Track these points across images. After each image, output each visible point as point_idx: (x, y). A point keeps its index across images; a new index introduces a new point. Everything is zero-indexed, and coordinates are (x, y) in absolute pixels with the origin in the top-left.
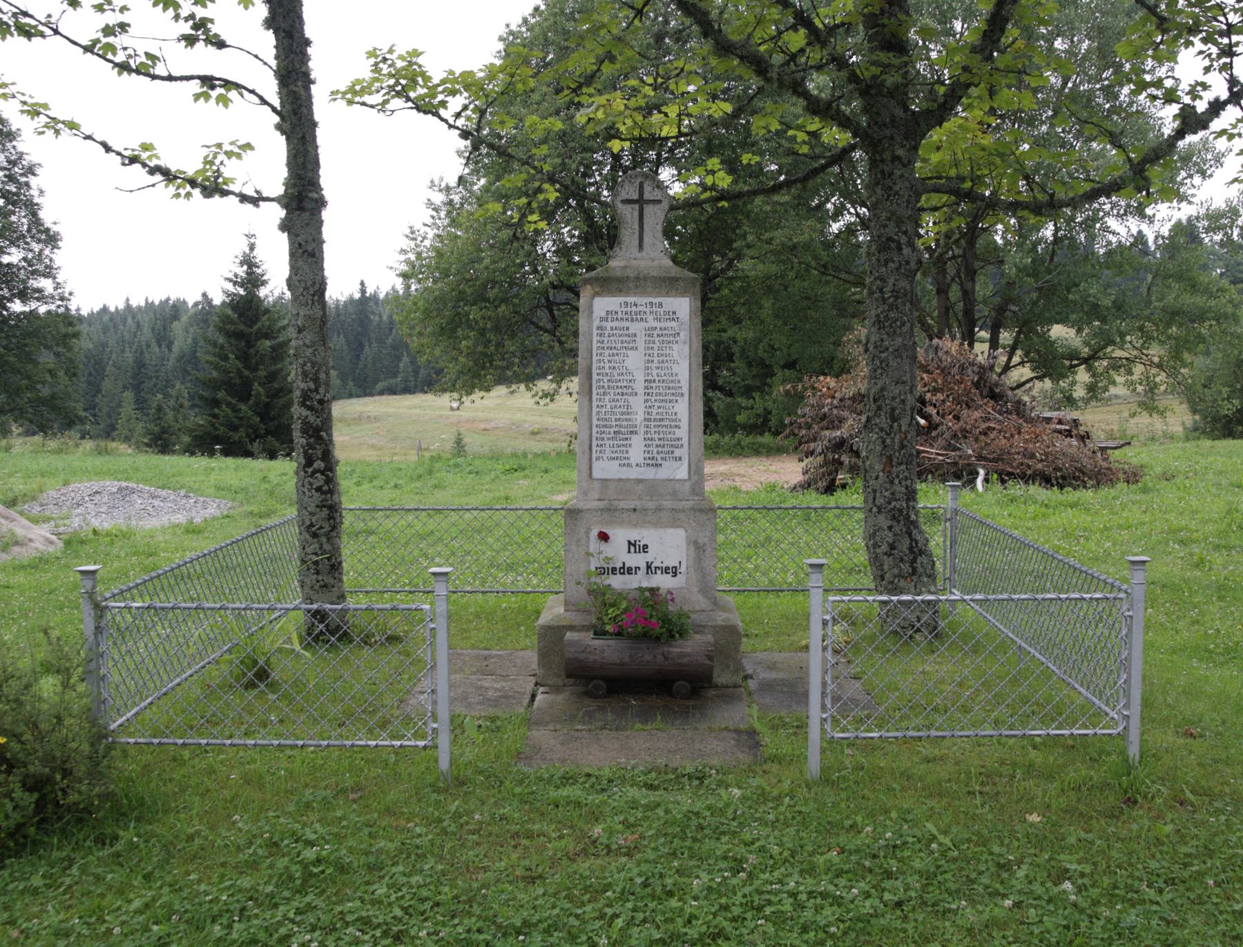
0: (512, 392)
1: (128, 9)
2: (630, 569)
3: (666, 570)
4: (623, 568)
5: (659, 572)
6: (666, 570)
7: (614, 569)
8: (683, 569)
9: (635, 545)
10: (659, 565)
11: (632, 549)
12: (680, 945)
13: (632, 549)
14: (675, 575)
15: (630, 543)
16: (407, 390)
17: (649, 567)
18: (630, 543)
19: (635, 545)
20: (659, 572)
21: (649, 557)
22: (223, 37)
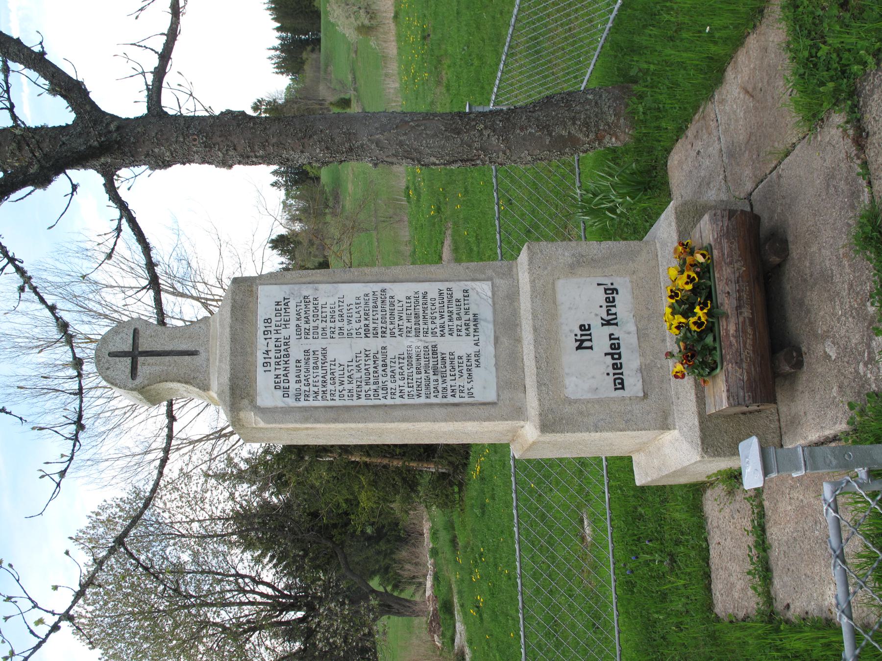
2: (612, 346)
3: (611, 302)
5: (613, 310)
6: (611, 302)
7: (615, 366)
8: (607, 281)
10: (604, 309)
13: (586, 344)
15: (578, 348)
18: (578, 348)
20: (613, 310)
21: (596, 324)
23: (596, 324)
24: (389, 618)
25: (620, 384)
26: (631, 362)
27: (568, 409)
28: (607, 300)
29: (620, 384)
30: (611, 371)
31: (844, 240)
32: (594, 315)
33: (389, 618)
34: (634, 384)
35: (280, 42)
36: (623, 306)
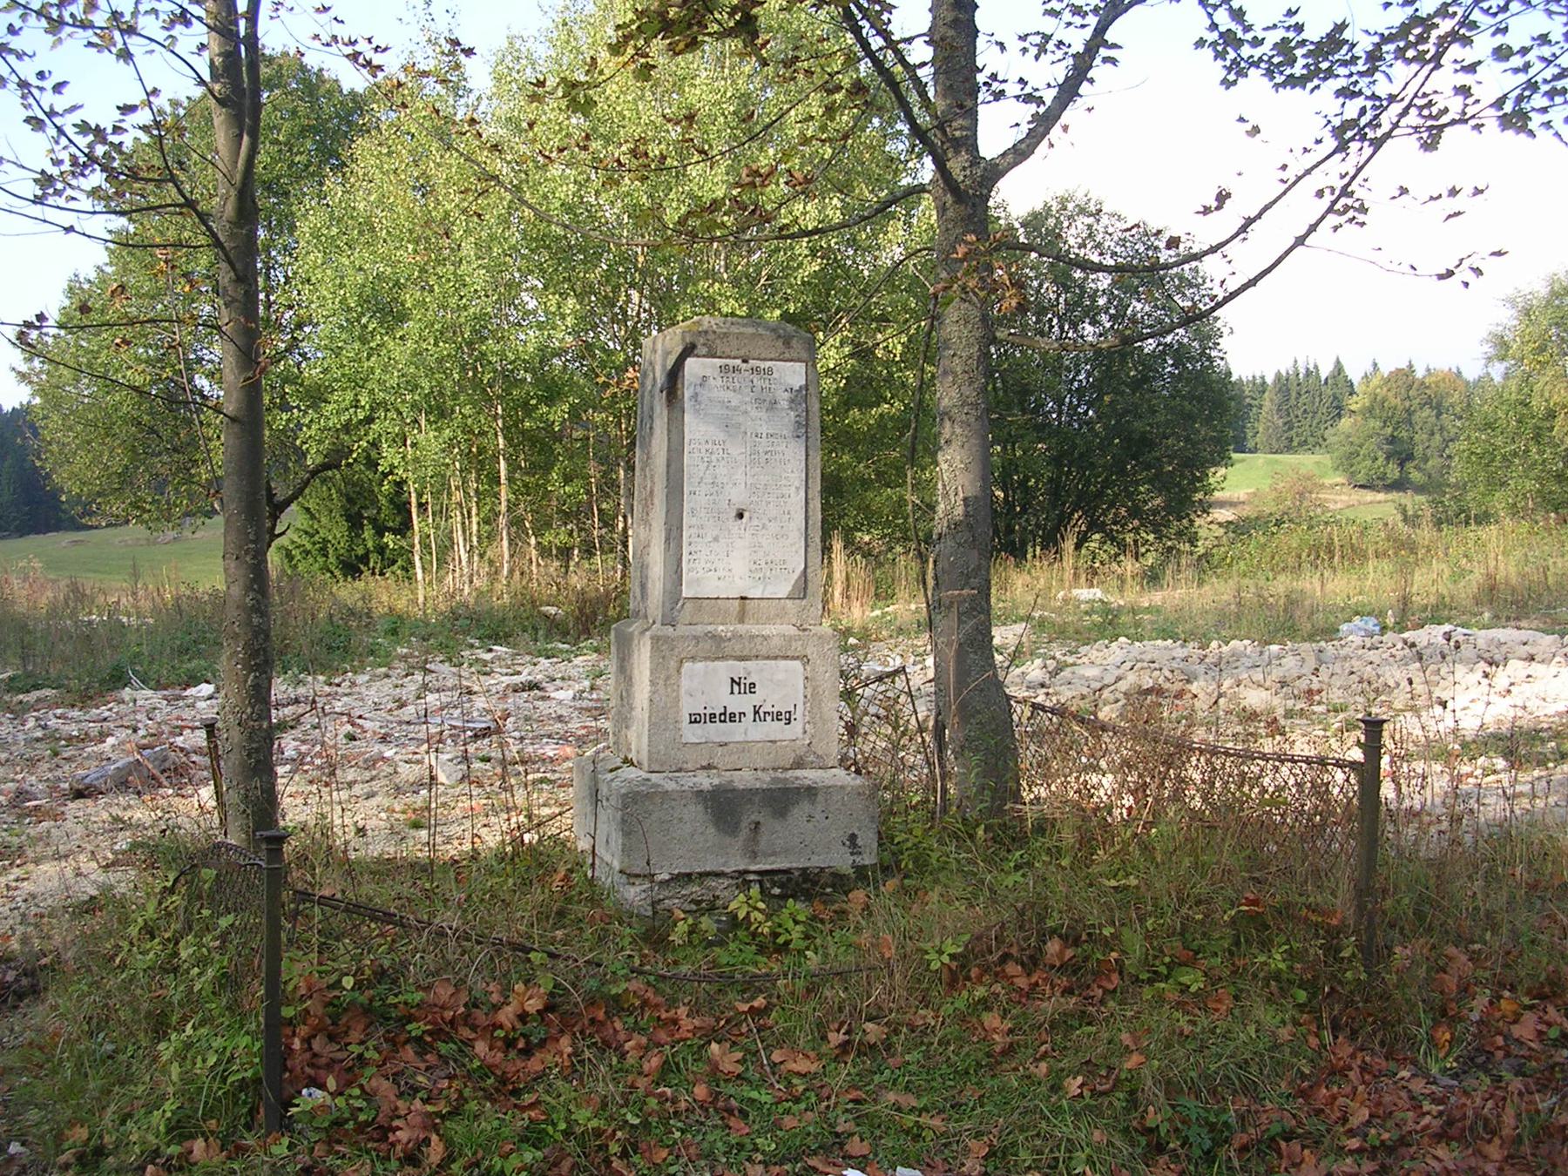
2: (732, 715)
3: (778, 716)
5: (769, 718)
6: (778, 716)
7: (713, 716)
8: (798, 715)
10: (770, 710)
13: (736, 688)
15: (733, 680)
17: (756, 712)
18: (733, 680)
20: (769, 718)
21: (755, 699)
23: (755, 699)
24: (1091, 81)
25: (695, 720)
26: (716, 731)
27: (673, 664)
28: (779, 714)
29: (695, 720)
30: (708, 712)
31: (712, 830)
32: (769, 697)
33: (1091, 81)
34: (692, 734)
35: (93, 276)
36: (773, 729)
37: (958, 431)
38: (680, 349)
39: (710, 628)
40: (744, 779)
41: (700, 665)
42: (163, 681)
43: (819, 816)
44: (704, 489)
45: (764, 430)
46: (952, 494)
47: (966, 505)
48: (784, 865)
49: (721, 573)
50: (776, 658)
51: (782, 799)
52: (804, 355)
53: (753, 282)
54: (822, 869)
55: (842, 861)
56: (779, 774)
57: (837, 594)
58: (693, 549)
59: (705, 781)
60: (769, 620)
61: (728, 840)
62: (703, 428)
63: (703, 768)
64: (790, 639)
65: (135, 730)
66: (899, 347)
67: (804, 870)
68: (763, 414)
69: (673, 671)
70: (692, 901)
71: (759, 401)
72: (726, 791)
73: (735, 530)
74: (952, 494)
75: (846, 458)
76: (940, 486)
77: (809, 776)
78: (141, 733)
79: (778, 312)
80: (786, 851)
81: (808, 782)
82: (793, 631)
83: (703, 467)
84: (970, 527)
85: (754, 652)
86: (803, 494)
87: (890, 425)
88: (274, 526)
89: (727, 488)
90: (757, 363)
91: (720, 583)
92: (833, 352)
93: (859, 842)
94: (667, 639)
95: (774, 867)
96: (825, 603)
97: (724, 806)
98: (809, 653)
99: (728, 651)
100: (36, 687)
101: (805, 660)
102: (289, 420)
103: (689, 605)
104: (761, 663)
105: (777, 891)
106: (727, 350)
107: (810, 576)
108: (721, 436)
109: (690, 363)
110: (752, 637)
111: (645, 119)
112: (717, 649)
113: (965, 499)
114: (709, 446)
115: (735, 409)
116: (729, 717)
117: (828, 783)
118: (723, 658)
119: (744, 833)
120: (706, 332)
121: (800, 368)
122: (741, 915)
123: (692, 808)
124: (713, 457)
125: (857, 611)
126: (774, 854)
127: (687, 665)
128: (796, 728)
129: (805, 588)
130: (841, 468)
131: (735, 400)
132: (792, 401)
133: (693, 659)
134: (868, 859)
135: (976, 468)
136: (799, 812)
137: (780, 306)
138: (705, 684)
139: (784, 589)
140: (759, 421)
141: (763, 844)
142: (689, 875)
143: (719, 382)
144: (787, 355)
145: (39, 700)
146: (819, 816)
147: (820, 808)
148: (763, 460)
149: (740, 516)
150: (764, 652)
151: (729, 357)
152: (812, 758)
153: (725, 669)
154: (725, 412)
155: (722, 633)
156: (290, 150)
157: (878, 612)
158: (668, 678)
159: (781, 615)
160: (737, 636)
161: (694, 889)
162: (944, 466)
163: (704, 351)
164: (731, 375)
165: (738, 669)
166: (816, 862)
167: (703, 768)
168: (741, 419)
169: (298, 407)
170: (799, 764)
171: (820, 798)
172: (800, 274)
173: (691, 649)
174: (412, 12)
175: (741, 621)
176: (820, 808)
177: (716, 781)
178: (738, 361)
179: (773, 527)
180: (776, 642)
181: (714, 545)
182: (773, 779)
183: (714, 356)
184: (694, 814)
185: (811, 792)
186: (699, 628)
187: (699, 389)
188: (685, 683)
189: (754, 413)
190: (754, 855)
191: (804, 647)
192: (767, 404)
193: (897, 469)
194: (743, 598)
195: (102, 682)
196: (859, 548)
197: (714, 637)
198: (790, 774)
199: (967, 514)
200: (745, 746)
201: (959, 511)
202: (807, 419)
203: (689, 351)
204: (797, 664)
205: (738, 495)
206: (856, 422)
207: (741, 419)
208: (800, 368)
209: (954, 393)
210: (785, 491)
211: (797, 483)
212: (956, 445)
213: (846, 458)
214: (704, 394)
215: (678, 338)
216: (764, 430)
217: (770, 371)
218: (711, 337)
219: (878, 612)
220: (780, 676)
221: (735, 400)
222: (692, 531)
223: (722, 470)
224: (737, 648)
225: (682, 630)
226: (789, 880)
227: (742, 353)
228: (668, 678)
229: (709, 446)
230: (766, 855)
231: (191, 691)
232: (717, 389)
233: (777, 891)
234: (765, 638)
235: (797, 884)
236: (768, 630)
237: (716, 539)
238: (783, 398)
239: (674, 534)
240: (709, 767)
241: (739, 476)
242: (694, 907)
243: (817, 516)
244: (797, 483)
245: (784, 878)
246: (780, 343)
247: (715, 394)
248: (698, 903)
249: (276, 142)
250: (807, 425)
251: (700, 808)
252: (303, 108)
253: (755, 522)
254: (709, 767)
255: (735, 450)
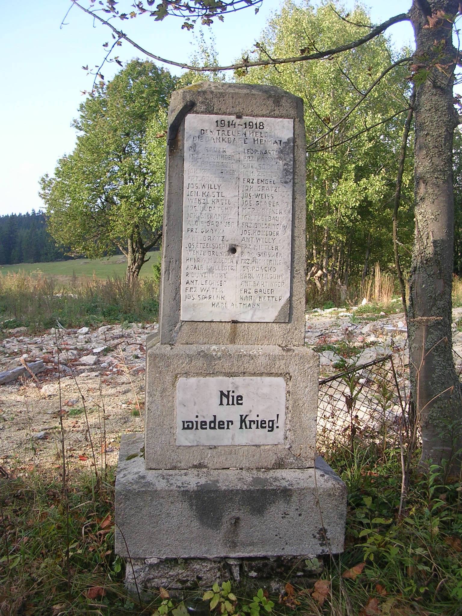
0: (40, 183)
1: (104, 45)
2: (221, 423)
3: (262, 424)
4: (214, 422)
5: (254, 426)
6: (262, 424)
7: (204, 423)
8: (281, 423)
9: (228, 397)
10: (255, 418)
11: (225, 400)
12: (342, 611)
13: (225, 400)
14: (271, 429)
15: (222, 392)
16: (52, 261)
17: (243, 421)
18: (222, 392)
19: (228, 397)
20: (254, 426)
21: (242, 410)
22: (160, 21)
23: (242, 410)
25: (188, 426)
27: (168, 378)
29: (188, 426)
30: (200, 420)
31: (196, 524)
32: (255, 408)
34: (185, 438)
37: (430, 191)
38: (180, 107)
39: (204, 348)
40: (230, 479)
41: (193, 380)
42: (73, 324)
43: (292, 513)
44: (200, 227)
45: (255, 176)
46: (425, 238)
47: (435, 246)
48: (261, 554)
49: (215, 301)
50: (261, 375)
51: (261, 498)
52: (292, 112)
53: (343, 153)
54: (295, 557)
55: (310, 550)
56: (261, 475)
57: (376, 291)
58: (190, 279)
59: (193, 480)
60: (257, 341)
61: (210, 532)
62: (200, 174)
63: (195, 467)
64: (274, 359)
65: (42, 350)
66: (408, 181)
67: (279, 558)
68: (256, 164)
69: (168, 385)
70: (179, 581)
71: (251, 151)
72: (210, 492)
73: (228, 263)
74: (425, 238)
75: (384, 230)
76: (416, 232)
77: (288, 476)
78: (44, 351)
79: (354, 166)
80: (263, 542)
81: (284, 484)
82: (278, 351)
83: (199, 208)
84: (438, 263)
85: (242, 369)
86: (289, 232)
87: (404, 216)
88: (144, 257)
89: (222, 226)
90: (250, 119)
91: (214, 309)
92: (378, 183)
93: (329, 535)
94: (163, 357)
95: (252, 555)
96: (371, 295)
97: (208, 503)
98: (291, 371)
99: (217, 368)
100: (18, 326)
101: (287, 376)
102: (145, 213)
103: (186, 327)
104: (248, 378)
105: (253, 574)
106: (224, 108)
107: (294, 304)
108: (215, 180)
109: (191, 119)
110: (240, 356)
111: (295, 81)
112: (209, 365)
113: (435, 242)
114: (206, 190)
115: (230, 157)
116: (218, 424)
117: (303, 485)
118: (214, 374)
119: (226, 526)
120: (204, 92)
121: (288, 123)
122: (213, 605)
123: (179, 505)
124: (210, 200)
125: (385, 300)
126: (252, 544)
127: (181, 380)
128: (278, 435)
129: (290, 314)
130: (382, 235)
131: (230, 150)
132: (281, 151)
133: (187, 374)
134: (337, 548)
135: (443, 219)
136: (275, 510)
137: (354, 163)
138: (197, 396)
139: (271, 314)
140: (252, 169)
141: (242, 536)
142: (176, 560)
143: (215, 135)
144: (277, 112)
145: (18, 332)
146: (292, 513)
147: (294, 507)
148: (254, 202)
149: (233, 250)
150: (251, 369)
151: (225, 113)
152: (292, 460)
153: (215, 384)
154: (221, 160)
155: (220, 351)
156: (149, 101)
157: (395, 300)
158: (164, 390)
159: (268, 337)
160: (227, 355)
161: (179, 571)
162: (419, 217)
163: (203, 108)
164: (226, 128)
165: (227, 383)
166: (289, 551)
167: (195, 467)
168: (235, 166)
169: (149, 207)
170: (280, 465)
171: (294, 498)
172: (363, 149)
173: (185, 366)
174: (196, 39)
175: (233, 341)
176: (294, 507)
177: (203, 481)
178: (233, 117)
179: (262, 261)
180: (262, 360)
181: (210, 277)
182: (256, 480)
183: (211, 112)
184: (180, 513)
185: (286, 493)
186: (194, 347)
187: (197, 141)
188: (179, 395)
189: (246, 161)
190: (234, 545)
191: (287, 365)
192: (258, 155)
193: (406, 235)
194: (235, 322)
195: (46, 325)
196: (390, 270)
197: (206, 356)
198: (272, 474)
199: (435, 253)
200: (232, 450)
201: (430, 250)
202: (294, 167)
203: (189, 107)
204: (280, 380)
205: (231, 233)
206: (388, 214)
207: (235, 166)
208: (288, 123)
209: (427, 163)
210: (274, 229)
211: (284, 223)
212: (428, 202)
213: (384, 230)
214: (202, 145)
215: (180, 97)
216: (255, 176)
217: (261, 126)
218: (210, 96)
219: (395, 300)
220: (266, 390)
221: (230, 150)
222: (189, 263)
223: (217, 211)
224: (227, 366)
225: (179, 348)
226: (265, 565)
227: (237, 110)
228: (164, 390)
229: (206, 190)
230: (244, 545)
231: (79, 331)
232: (214, 141)
233: (253, 574)
234: (252, 357)
235: (272, 569)
236: (256, 350)
237: (211, 270)
238: (273, 149)
239: (173, 265)
240: (200, 466)
241: (232, 215)
242: (179, 585)
243: (302, 252)
244: (284, 223)
245: (260, 563)
246: (270, 102)
247: (212, 145)
248: (183, 582)
249: (142, 98)
250: (294, 173)
251: (186, 505)
252: (153, 83)
253: (246, 256)
254: (200, 466)
255: (230, 193)
